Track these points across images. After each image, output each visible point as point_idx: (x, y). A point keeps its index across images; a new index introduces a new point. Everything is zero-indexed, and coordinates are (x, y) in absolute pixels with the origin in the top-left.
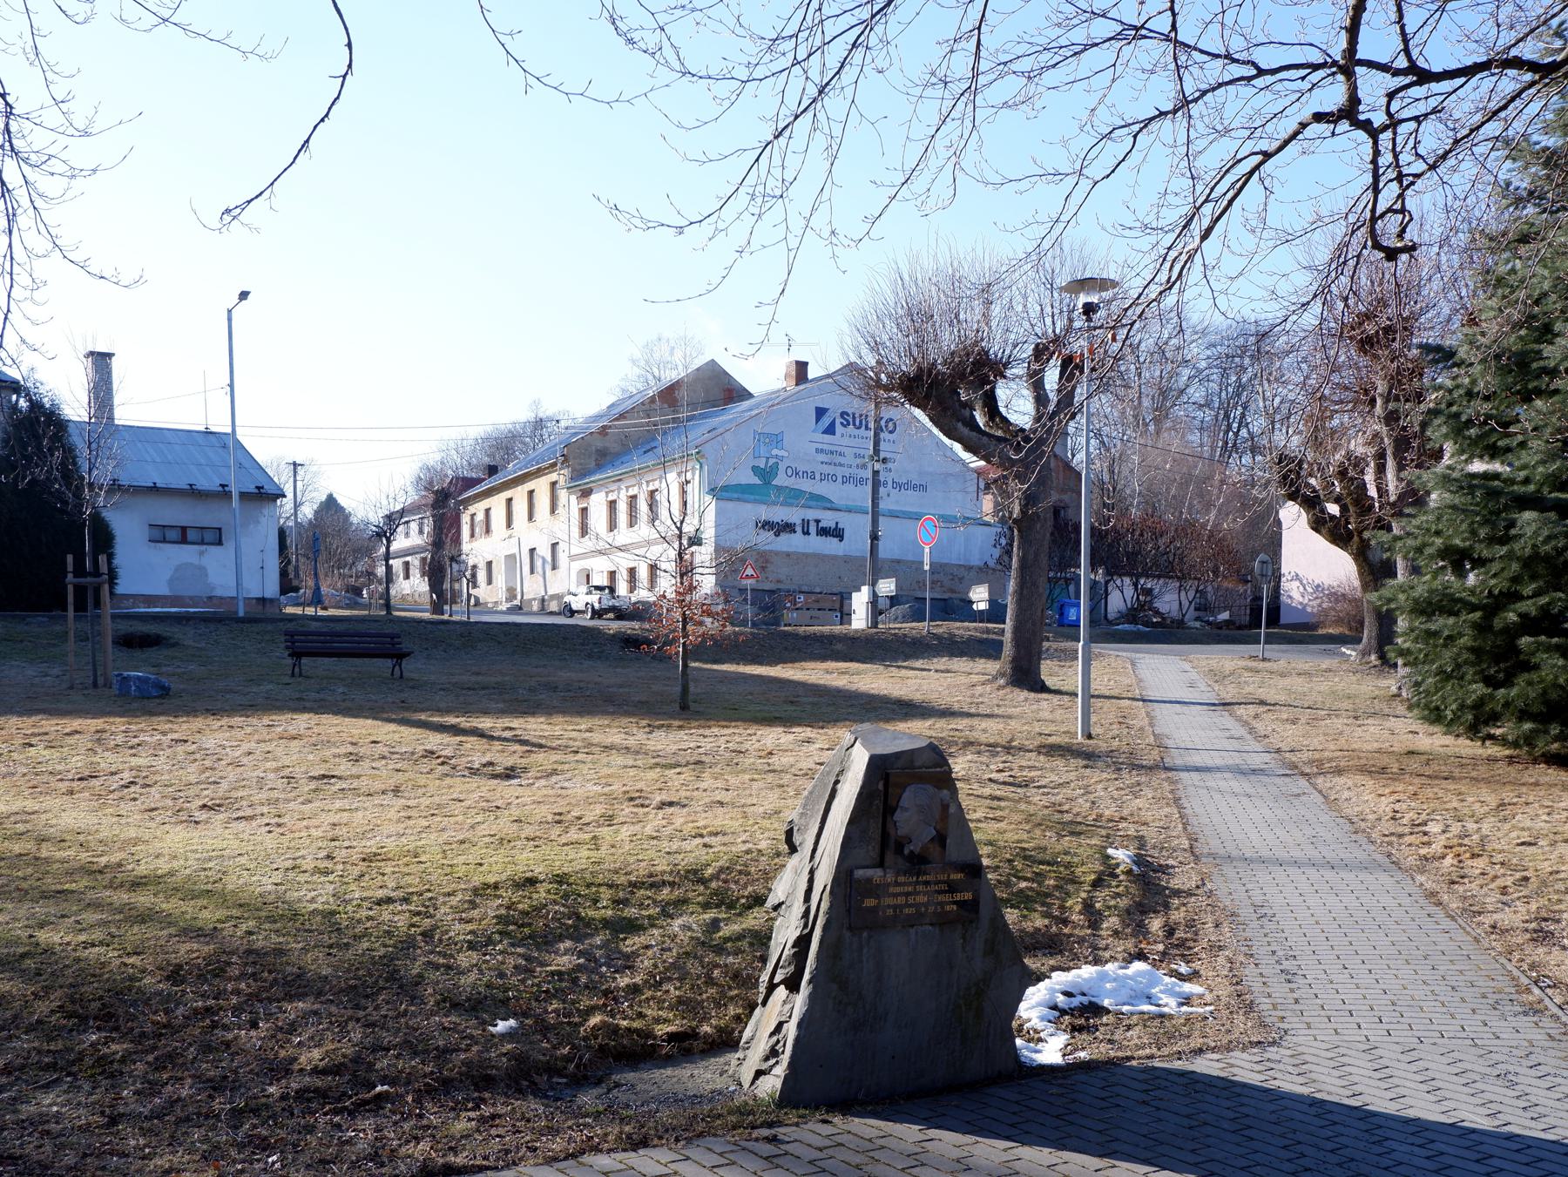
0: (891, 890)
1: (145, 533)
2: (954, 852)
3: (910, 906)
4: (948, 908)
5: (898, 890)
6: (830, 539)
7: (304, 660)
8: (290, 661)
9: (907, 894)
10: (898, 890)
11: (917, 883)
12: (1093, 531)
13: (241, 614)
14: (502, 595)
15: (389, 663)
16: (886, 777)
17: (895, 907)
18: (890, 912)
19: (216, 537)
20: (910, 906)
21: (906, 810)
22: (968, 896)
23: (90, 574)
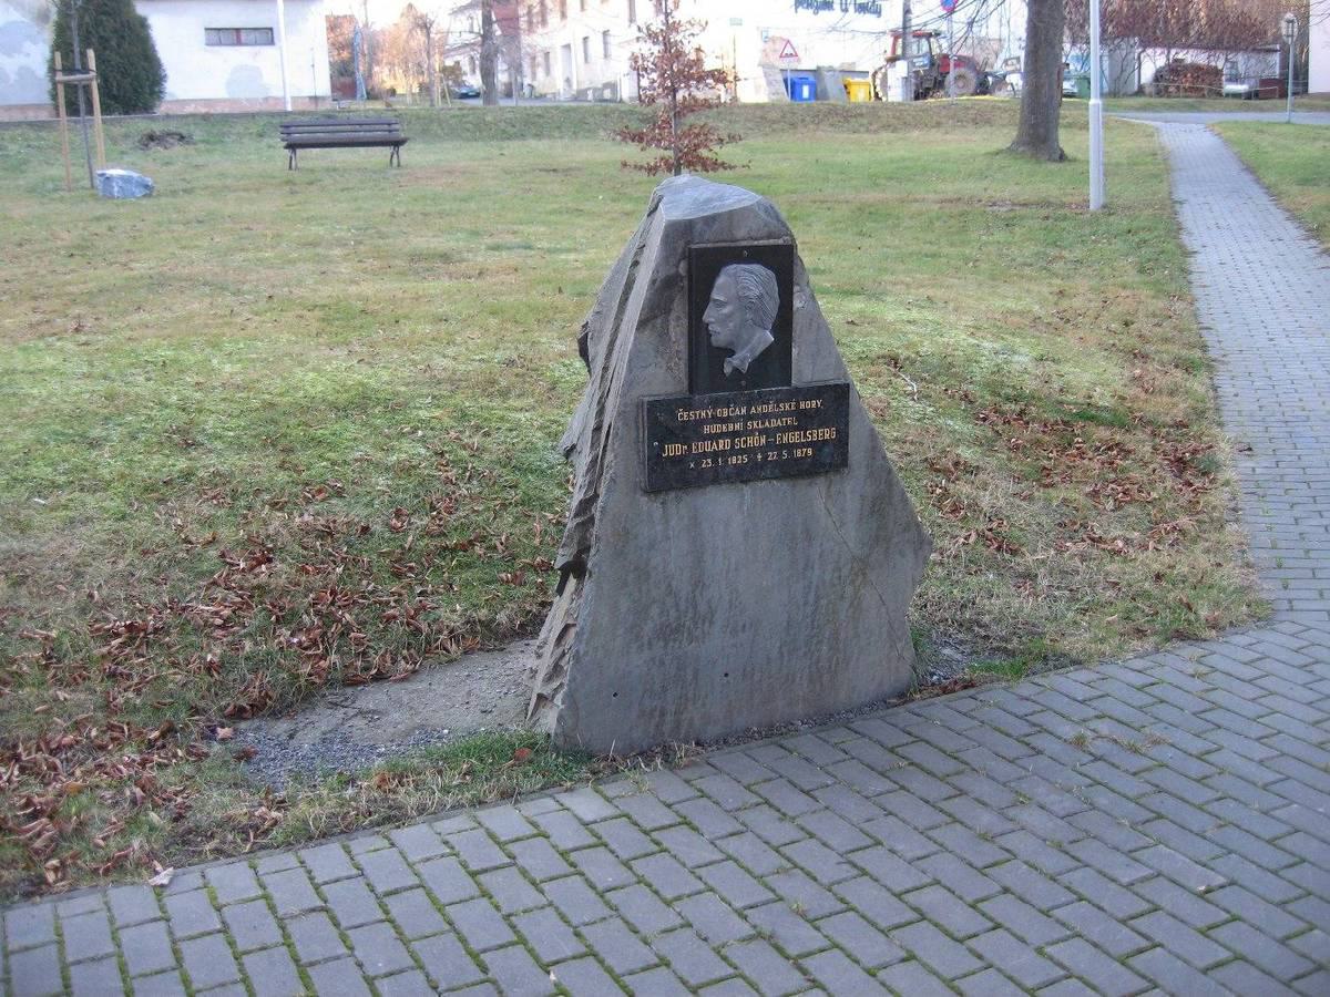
0: (707, 430)
1: (202, 35)
2: (805, 370)
3: (742, 451)
4: (798, 453)
5: (716, 428)
6: (868, 16)
7: (299, 151)
8: (287, 152)
9: (734, 435)
10: (716, 428)
11: (749, 417)
12: (1295, 62)
13: (1095, 197)
14: (560, 85)
15: (387, 150)
16: (697, 260)
17: (715, 455)
18: (707, 463)
19: (266, 36)
20: (742, 451)
21: (721, 304)
22: (828, 433)
23: (79, 72)
